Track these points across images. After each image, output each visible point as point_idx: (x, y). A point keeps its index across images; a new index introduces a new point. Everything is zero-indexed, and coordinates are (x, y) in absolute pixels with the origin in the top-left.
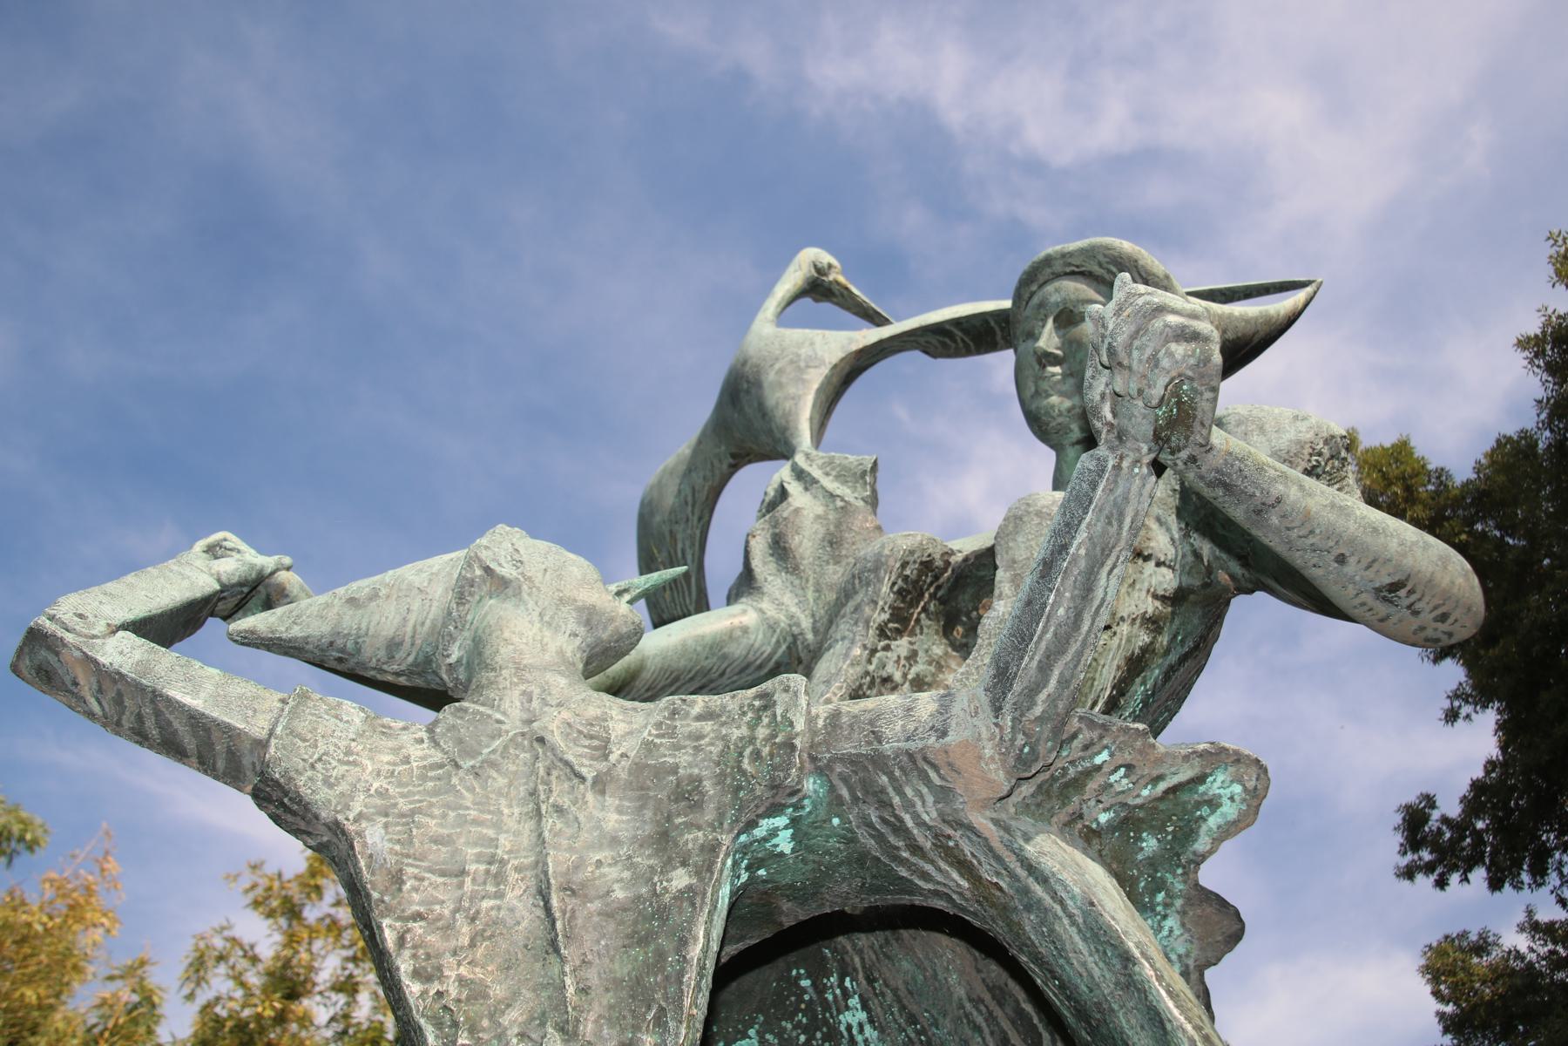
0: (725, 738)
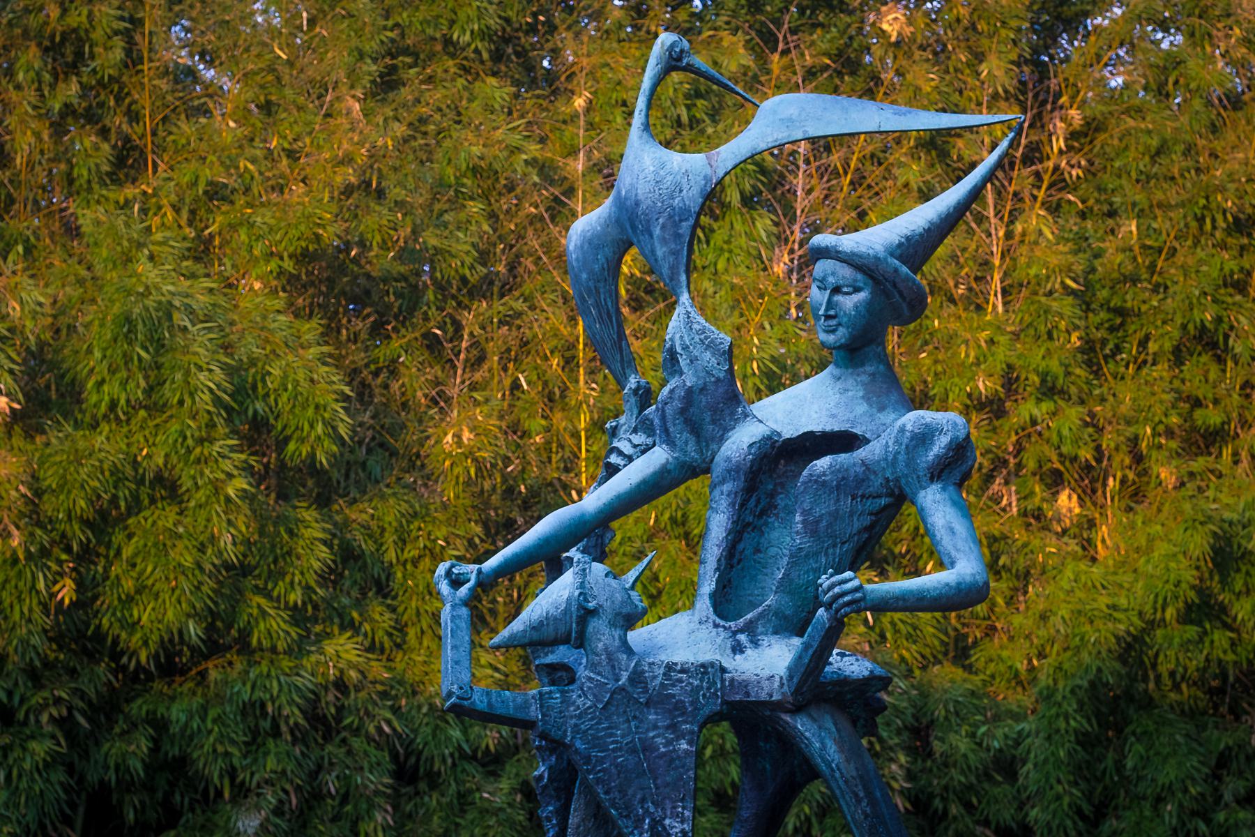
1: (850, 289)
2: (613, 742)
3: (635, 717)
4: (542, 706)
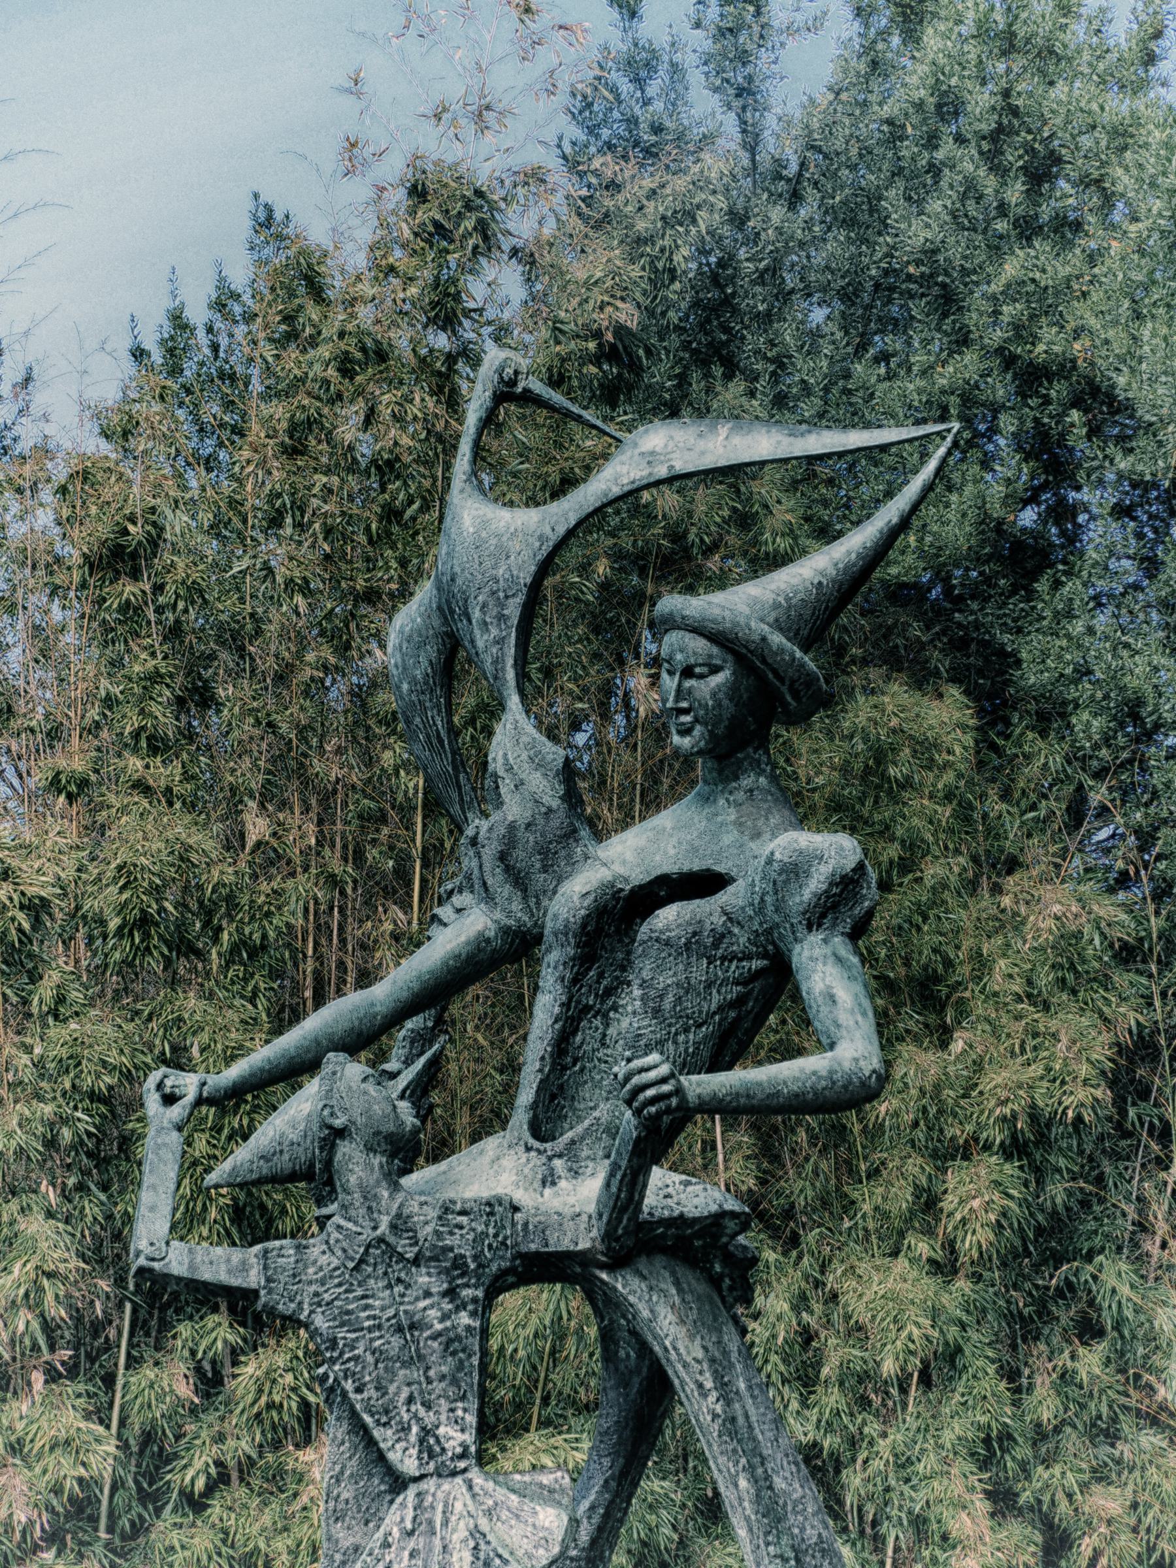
0: (474, 1230)
1: (705, 670)
2: (368, 1318)
3: (399, 1280)
4: (266, 1267)
